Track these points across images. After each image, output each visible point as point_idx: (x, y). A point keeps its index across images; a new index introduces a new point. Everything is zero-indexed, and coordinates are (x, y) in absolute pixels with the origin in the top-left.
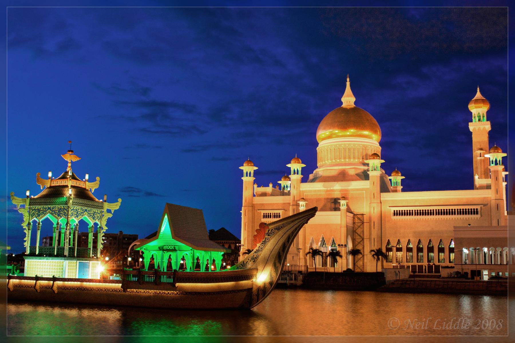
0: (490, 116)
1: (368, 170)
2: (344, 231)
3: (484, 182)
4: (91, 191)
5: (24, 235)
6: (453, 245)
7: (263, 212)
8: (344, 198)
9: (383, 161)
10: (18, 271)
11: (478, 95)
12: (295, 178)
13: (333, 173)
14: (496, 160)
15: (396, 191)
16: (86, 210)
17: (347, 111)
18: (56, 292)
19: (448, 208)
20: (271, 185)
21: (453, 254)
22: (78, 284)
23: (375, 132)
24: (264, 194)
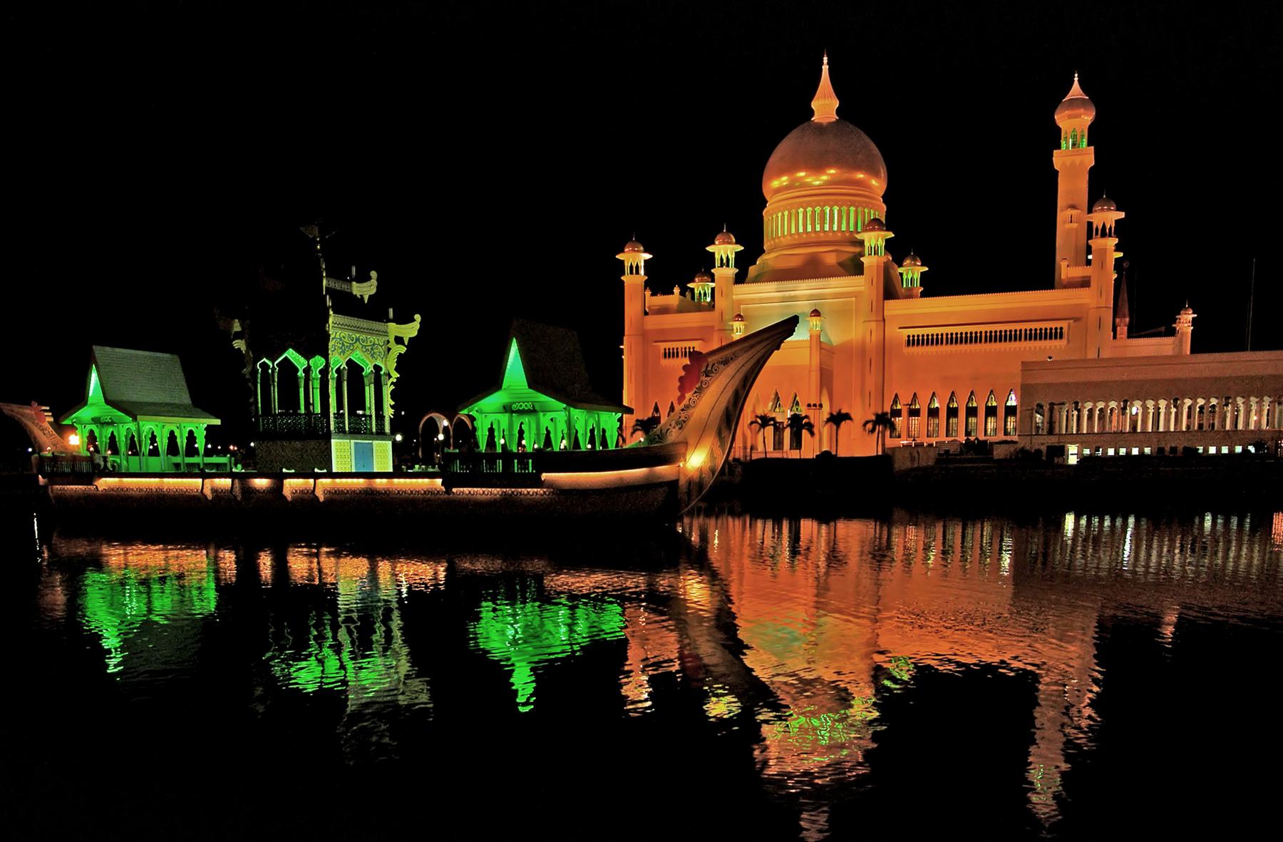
0: (1095, 135)
2: (815, 378)
3: (1079, 272)
6: (1012, 402)
11: (1076, 90)
12: (725, 273)
13: (794, 263)
15: (910, 296)
16: (358, 340)
17: (821, 129)
18: (322, 499)
20: (677, 290)
21: (1013, 419)
22: (360, 483)
23: (876, 174)
24: (664, 310)
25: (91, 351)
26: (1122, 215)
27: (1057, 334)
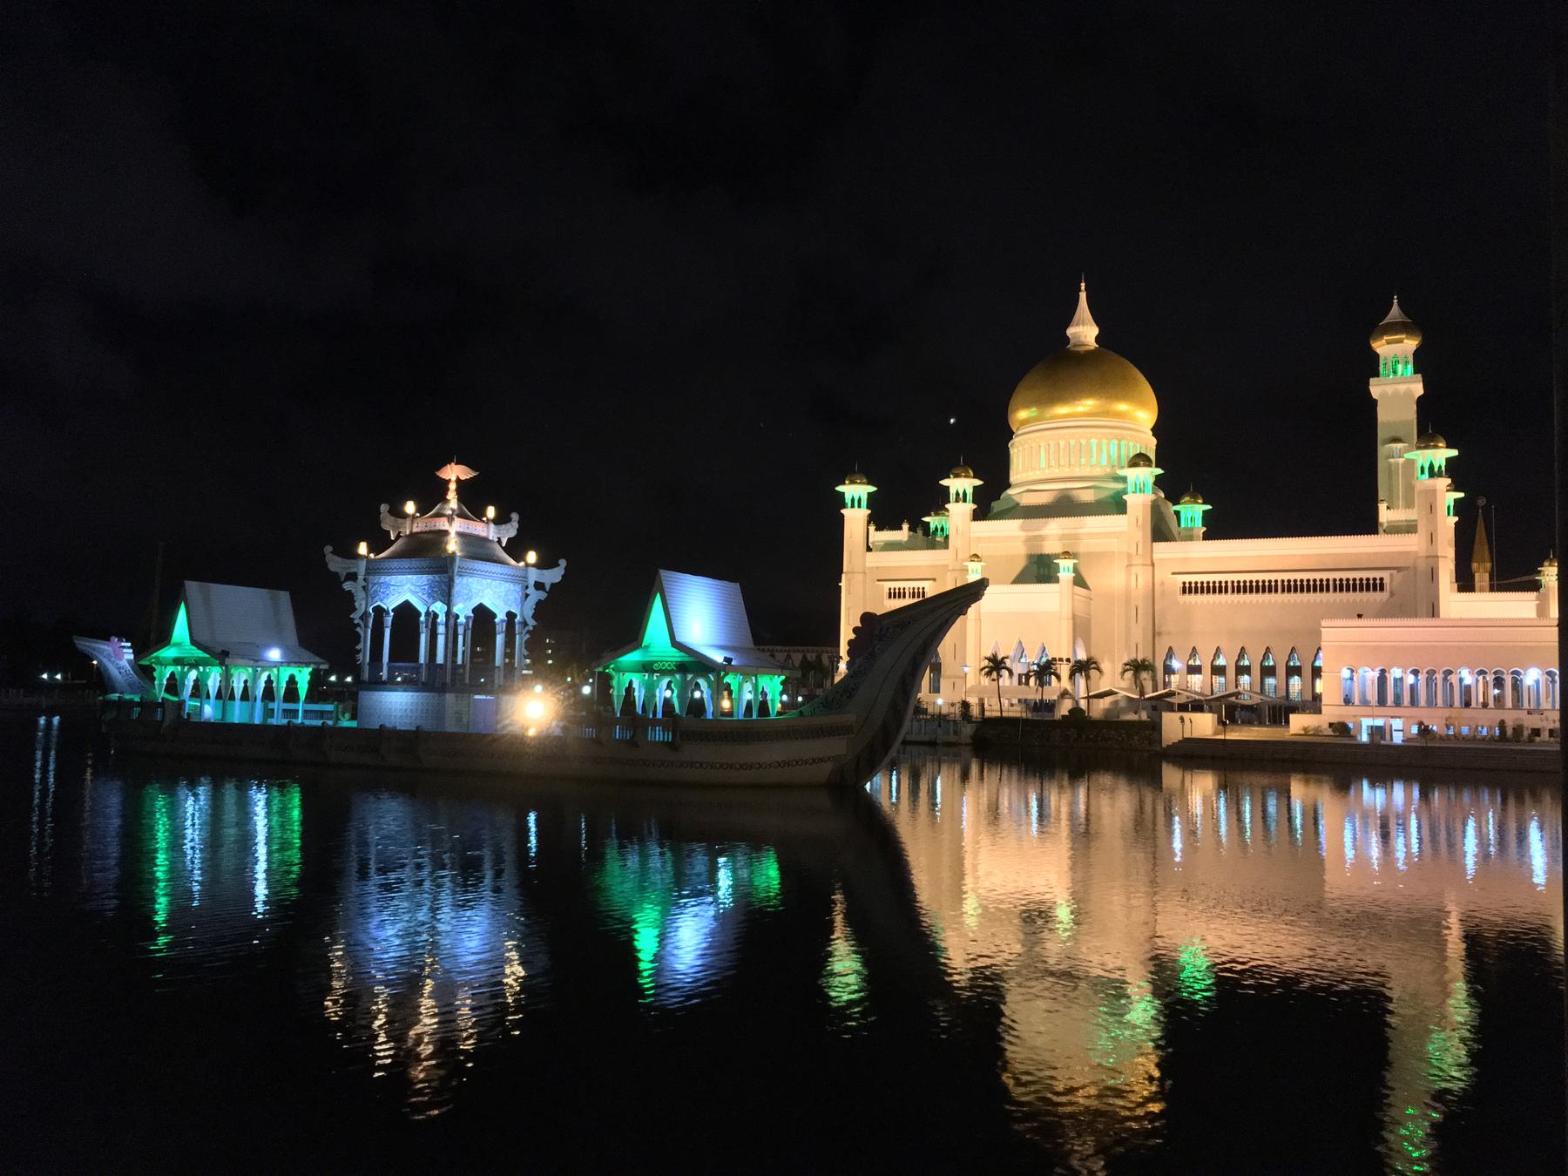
0: (1422, 361)
1: (1125, 492)
2: (1066, 628)
4: (499, 542)
5: (357, 638)
7: (888, 585)
8: (1067, 554)
9: (1160, 471)
10: (347, 716)
11: (1395, 312)
14: (1431, 467)
15: (1190, 538)
19: (1261, 577)
20: (905, 527)
25: (182, 585)
26: (1454, 453)
27: (1378, 586)
